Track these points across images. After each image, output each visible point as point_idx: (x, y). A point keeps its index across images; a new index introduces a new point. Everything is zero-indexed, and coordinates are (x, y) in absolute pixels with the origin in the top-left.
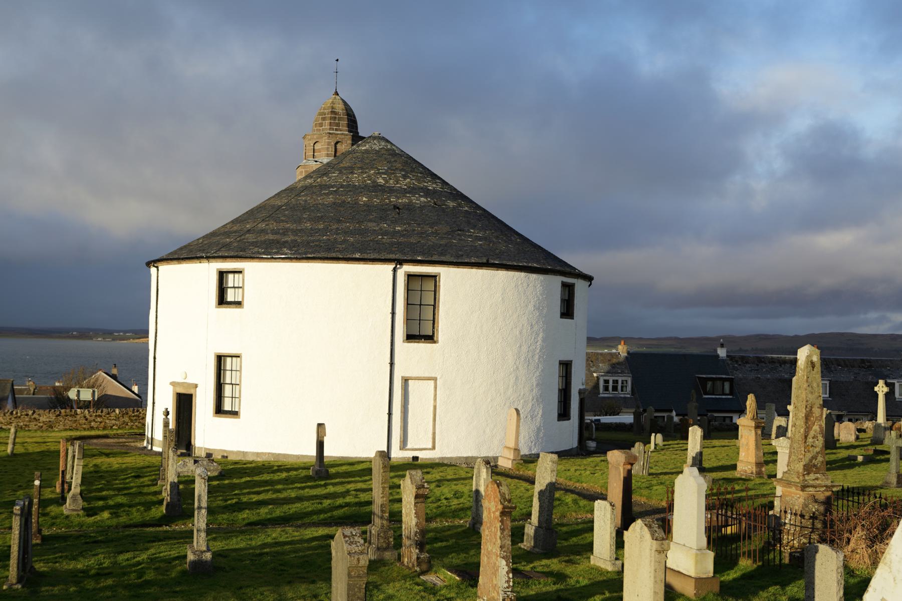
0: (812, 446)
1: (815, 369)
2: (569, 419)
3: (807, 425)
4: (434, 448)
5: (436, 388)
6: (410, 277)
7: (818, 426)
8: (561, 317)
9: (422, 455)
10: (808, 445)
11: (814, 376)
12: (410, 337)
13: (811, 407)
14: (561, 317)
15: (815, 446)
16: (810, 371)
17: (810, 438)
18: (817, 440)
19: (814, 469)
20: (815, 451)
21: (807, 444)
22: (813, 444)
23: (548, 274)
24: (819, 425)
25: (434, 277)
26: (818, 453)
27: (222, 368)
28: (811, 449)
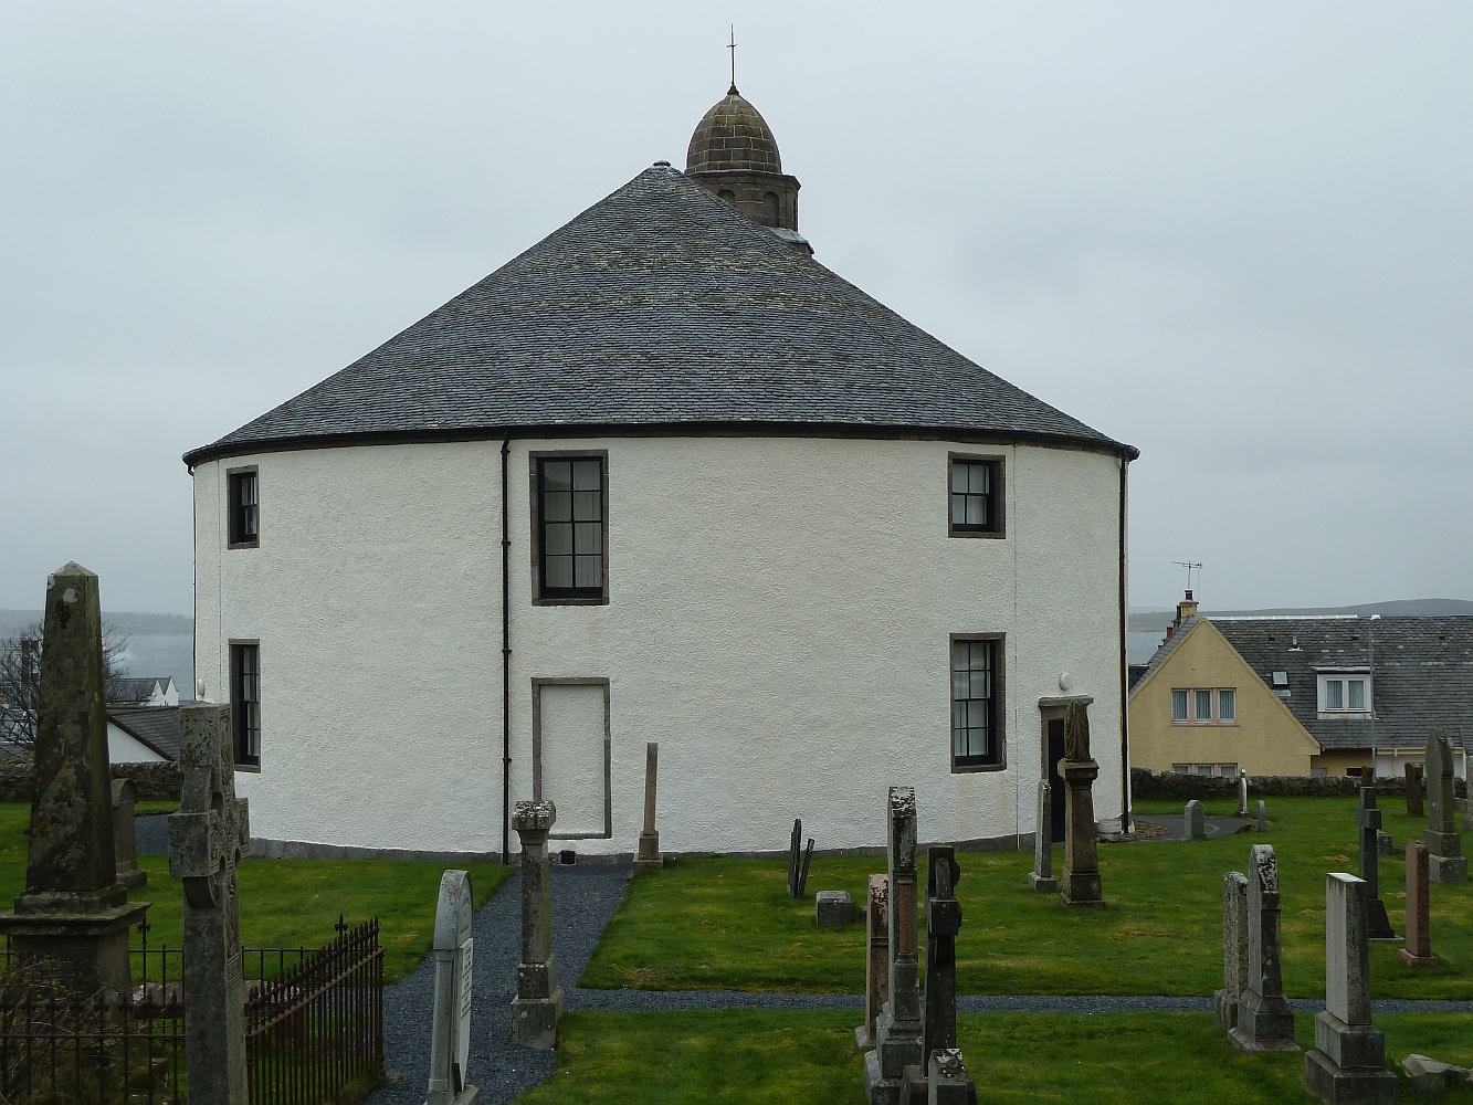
0: (54, 820)
1: (68, 625)
2: (1003, 768)
3: (42, 766)
4: (608, 834)
5: (607, 702)
6: (540, 462)
7: (72, 770)
8: (951, 535)
9: (583, 848)
10: (42, 819)
11: (66, 640)
12: (548, 593)
13: (56, 722)
14: (951, 535)
15: (61, 819)
16: (55, 629)
17: (47, 801)
18: (70, 805)
19: (58, 881)
20: (62, 833)
21: (41, 814)
22: (55, 815)
23: (1093, 452)
24: (75, 766)
25: (600, 459)
26: (69, 839)
27: (988, 674)
28: (50, 828)
